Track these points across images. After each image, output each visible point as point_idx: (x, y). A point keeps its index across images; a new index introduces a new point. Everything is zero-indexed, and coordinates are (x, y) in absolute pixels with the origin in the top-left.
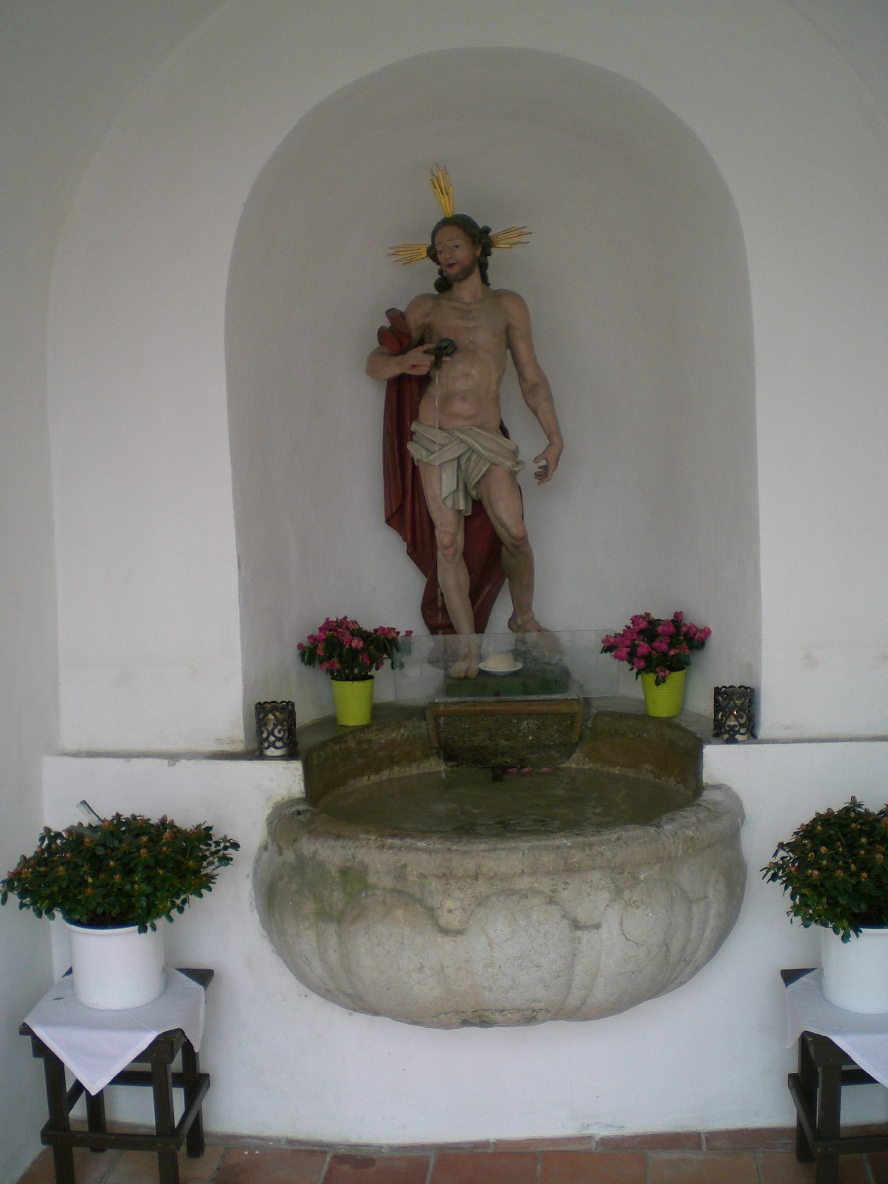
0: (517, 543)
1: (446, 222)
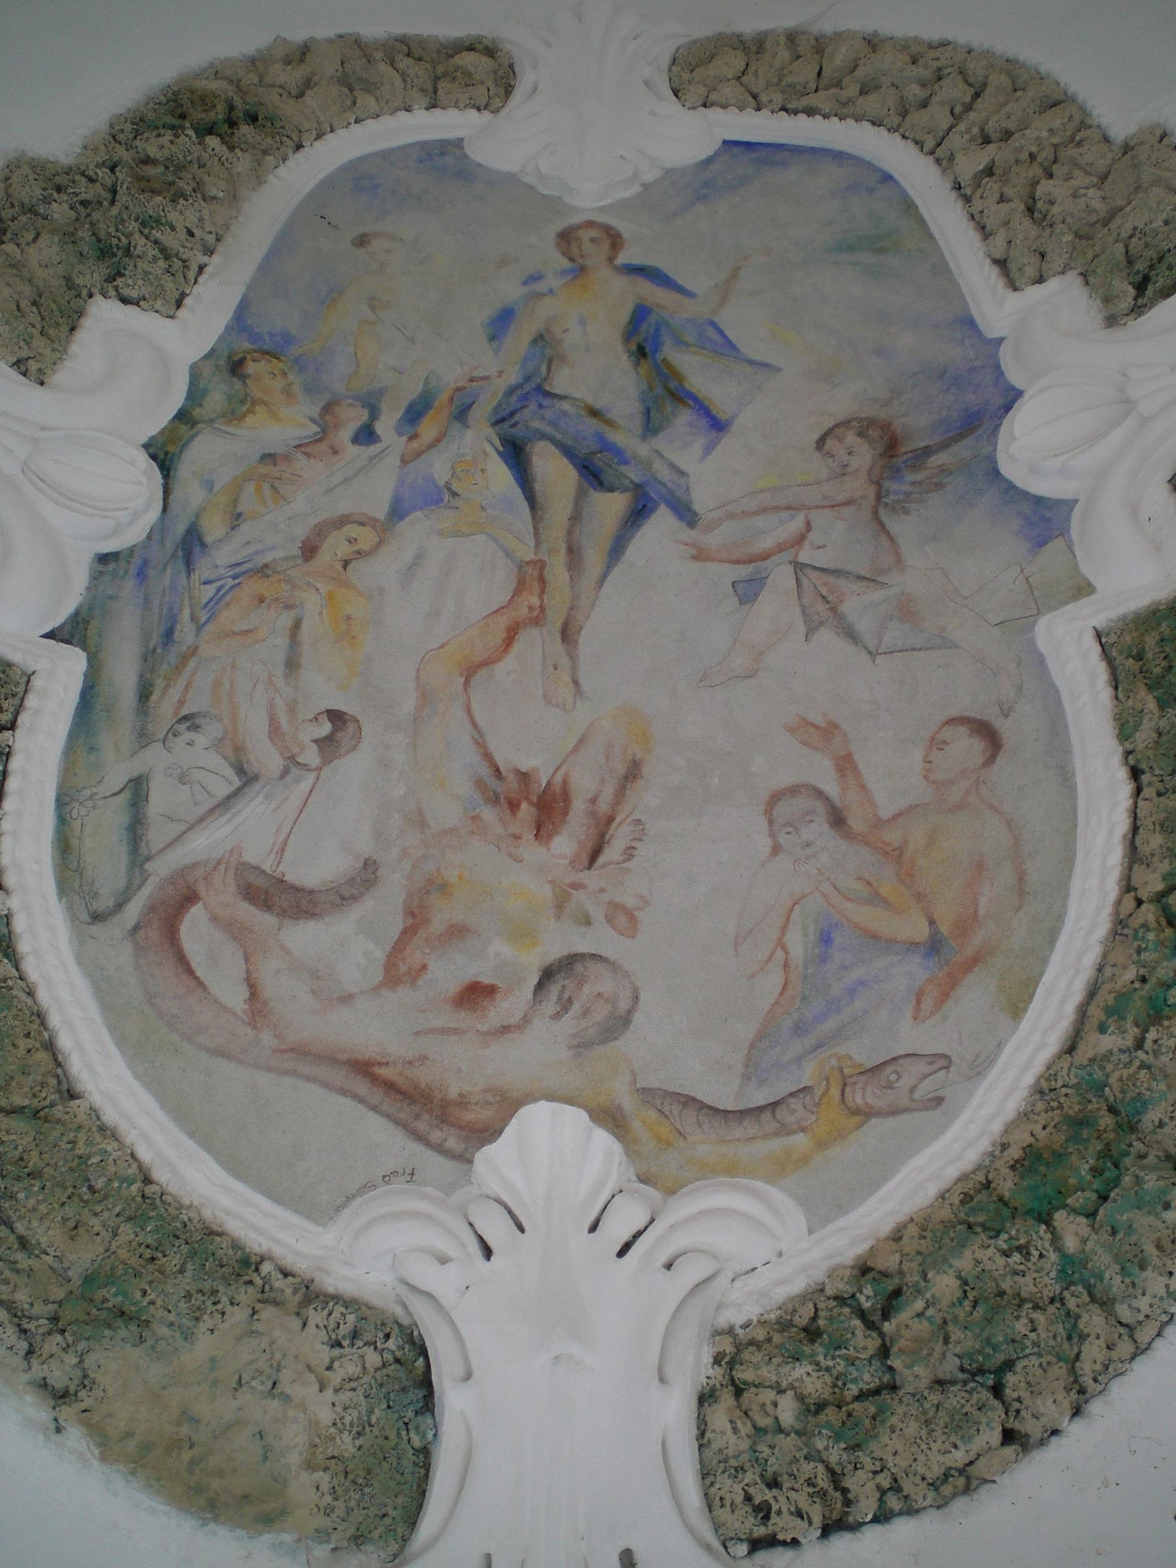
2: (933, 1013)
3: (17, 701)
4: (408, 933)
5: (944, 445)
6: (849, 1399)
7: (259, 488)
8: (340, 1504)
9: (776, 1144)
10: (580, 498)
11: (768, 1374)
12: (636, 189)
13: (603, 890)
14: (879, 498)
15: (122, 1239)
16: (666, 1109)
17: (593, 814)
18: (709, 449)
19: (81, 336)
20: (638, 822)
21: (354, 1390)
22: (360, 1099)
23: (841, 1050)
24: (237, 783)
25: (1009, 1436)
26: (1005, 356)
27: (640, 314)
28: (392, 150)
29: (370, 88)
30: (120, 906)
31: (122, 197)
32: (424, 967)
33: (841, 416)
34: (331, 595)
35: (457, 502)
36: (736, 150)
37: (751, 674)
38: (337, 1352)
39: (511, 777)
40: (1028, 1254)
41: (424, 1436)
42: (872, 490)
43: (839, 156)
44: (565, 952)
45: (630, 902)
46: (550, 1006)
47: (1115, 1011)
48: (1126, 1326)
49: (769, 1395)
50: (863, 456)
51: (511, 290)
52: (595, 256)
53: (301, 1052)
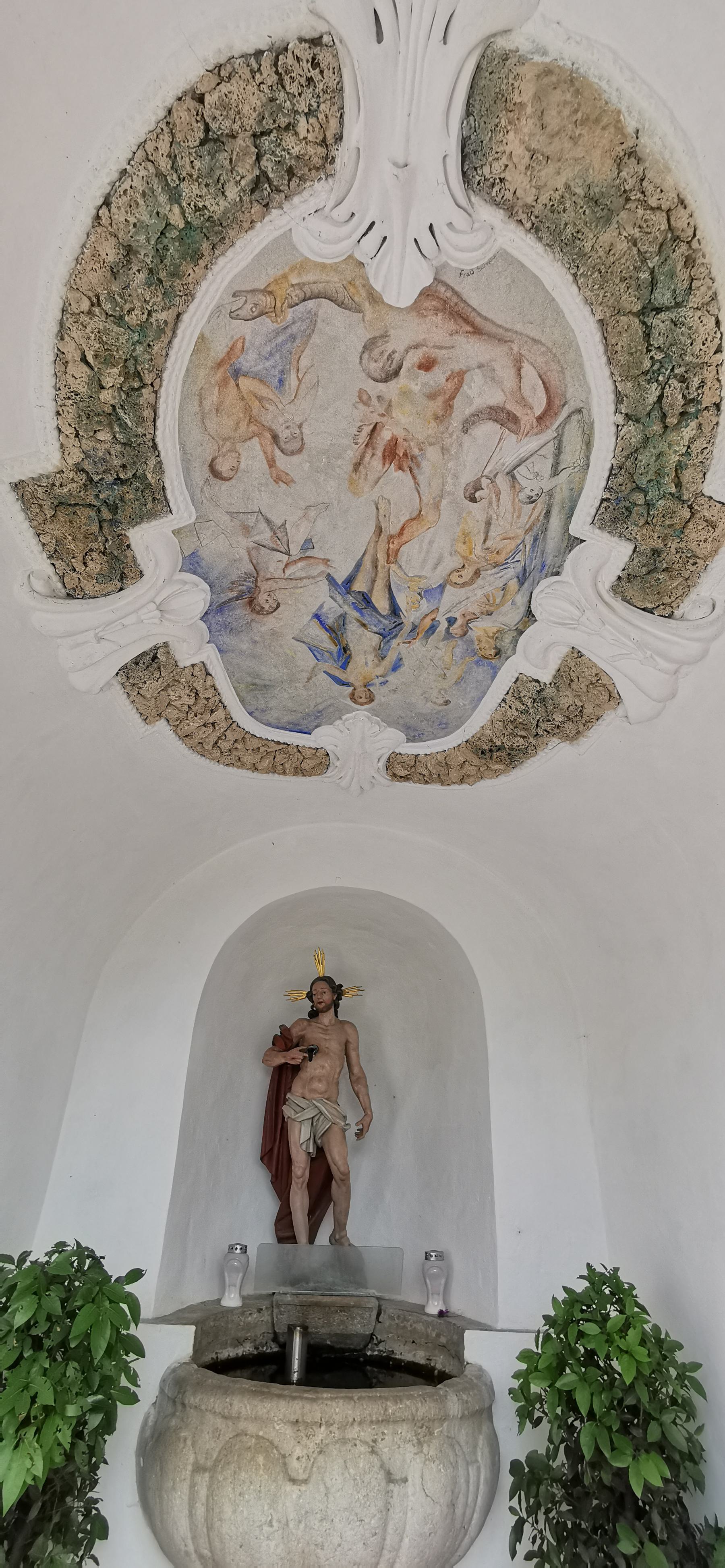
0: (343, 1177)
1: (319, 979)
2: (237, 340)
3: (599, 512)
4: (452, 398)
5: (231, 600)
6: (275, 131)
7: (494, 600)
8: (511, 81)
9: (305, 279)
10: (371, 590)
11: (311, 150)
12: (344, 718)
13: (372, 412)
14: (256, 580)
15: (590, 244)
16: (351, 301)
17: (374, 449)
18: (321, 607)
19: (556, 667)
20: (356, 444)
21: (497, 153)
22: (479, 314)
23: (276, 325)
24: (515, 471)
25: (201, 99)
26: (207, 637)
27: (344, 667)
28: (433, 739)
29: (439, 764)
30: (569, 416)
31: (534, 722)
32: (447, 380)
33: (270, 616)
34: (471, 553)
35: (418, 590)
36: (306, 730)
37: (308, 507)
38: (502, 176)
39: (406, 468)
40: (195, 206)
41: (468, 123)
42: (259, 585)
43: (268, 724)
44: (388, 383)
45: (361, 406)
46: (397, 357)
47: (161, 331)
48: (149, 160)
49: (310, 137)
50: (262, 599)
51: (392, 678)
52: (361, 691)
53: (501, 340)
